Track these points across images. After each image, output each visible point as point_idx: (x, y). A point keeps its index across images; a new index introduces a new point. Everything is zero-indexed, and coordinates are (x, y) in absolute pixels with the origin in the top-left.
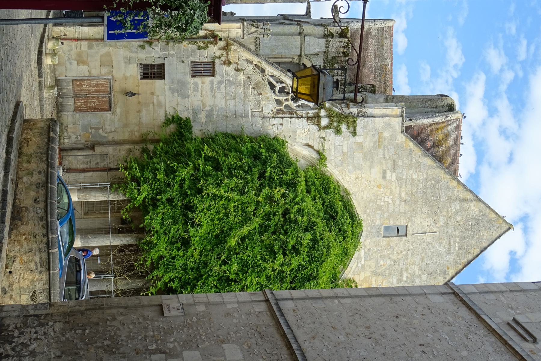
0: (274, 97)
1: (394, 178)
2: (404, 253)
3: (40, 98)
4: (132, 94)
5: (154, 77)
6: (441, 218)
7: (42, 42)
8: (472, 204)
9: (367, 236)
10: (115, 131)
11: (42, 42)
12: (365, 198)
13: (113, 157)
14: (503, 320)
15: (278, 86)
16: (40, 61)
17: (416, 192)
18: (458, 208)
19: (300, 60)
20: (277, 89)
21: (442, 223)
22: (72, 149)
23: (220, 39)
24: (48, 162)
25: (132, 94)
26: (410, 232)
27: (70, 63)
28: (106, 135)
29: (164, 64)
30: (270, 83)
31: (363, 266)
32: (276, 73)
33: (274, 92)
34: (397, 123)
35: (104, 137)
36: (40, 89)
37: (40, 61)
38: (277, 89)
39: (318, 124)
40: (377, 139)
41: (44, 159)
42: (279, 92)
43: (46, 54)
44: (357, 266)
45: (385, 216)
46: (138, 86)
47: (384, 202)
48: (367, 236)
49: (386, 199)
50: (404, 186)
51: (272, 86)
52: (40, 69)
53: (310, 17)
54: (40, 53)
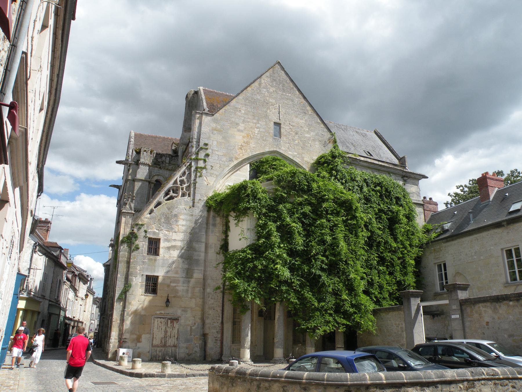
0: (179, 197)
1: (243, 125)
2: (291, 127)
3: (173, 377)
4: (168, 301)
5: (156, 284)
6: (271, 100)
7: (122, 372)
8: (263, 81)
9: (280, 148)
10: (194, 317)
11: (122, 372)
12: (254, 146)
13: (213, 319)
14: (181, 241)
15: (171, 193)
16: (139, 376)
17: (253, 113)
18: (265, 90)
19: (153, 183)
20: (174, 195)
21: (274, 101)
22: (205, 351)
23: (133, 230)
24: (272, 380)
25: (168, 301)
26: (278, 121)
27: (139, 348)
28: (197, 324)
29: (147, 276)
30: (168, 199)
31: (299, 154)
32: (162, 193)
33: (176, 197)
34: (206, 119)
35: (198, 325)
36: (163, 376)
37: (139, 376)
38: (174, 195)
39: (202, 168)
40: (215, 132)
41: (267, 384)
42: (177, 193)
43: (132, 369)
44: (298, 157)
45: (267, 134)
46: (161, 296)
47: (258, 134)
48: (280, 148)
49: (256, 132)
50: (249, 120)
51: (172, 198)
52: (146, 376)
53: (121, 186)
54: (131, 375)
